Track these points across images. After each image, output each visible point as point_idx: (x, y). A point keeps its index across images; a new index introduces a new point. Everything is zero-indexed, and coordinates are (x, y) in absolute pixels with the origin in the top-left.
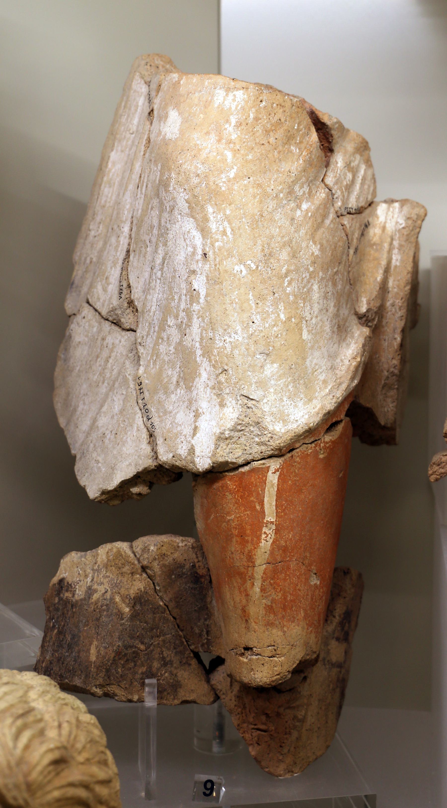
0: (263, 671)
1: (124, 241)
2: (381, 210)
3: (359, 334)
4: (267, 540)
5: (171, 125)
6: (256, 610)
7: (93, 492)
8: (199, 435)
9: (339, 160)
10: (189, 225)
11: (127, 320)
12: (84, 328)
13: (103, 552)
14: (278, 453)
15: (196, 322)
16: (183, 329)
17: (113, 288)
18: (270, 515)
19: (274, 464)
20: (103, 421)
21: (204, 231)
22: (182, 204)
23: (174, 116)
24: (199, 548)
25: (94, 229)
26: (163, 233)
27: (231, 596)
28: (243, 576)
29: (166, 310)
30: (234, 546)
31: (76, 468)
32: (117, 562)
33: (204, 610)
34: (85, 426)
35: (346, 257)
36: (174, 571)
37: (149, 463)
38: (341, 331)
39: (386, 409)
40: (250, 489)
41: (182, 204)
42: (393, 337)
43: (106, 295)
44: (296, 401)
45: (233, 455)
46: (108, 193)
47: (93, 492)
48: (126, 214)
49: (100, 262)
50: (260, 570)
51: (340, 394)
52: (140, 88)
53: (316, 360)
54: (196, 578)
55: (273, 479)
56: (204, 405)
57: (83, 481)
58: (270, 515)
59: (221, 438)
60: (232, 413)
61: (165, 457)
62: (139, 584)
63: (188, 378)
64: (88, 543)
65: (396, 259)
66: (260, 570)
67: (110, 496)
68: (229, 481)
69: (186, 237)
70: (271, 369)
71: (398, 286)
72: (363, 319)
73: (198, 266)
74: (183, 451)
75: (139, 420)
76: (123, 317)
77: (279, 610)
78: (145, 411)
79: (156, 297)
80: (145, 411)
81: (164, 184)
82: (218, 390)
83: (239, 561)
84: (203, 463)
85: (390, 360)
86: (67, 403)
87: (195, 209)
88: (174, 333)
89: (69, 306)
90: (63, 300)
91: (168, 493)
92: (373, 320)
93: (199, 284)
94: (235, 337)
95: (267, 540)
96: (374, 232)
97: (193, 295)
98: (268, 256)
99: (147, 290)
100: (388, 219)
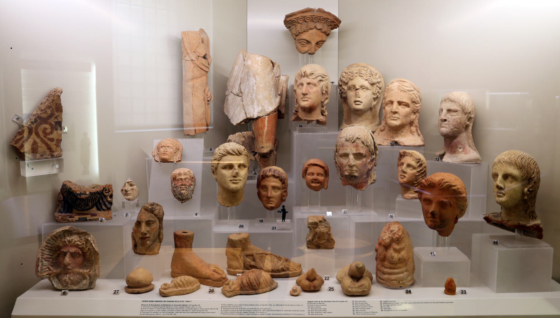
0: (265, 151)
1: (239, 82)
2: (281, 77)
3: (279, 97)
4: (266, 129)
5: (249, 63)
6: (264, 141)
7: (235, 124)
8: (254, 113)
9: (275, 68)
10: (253, 78)
11: (240, 95)
12: (231, 97)
13: (237, 134)
14: (268, 115)
15: (254, 95)
16: (251, 96)
17: (237, 89)
18: (266, 125)
19: (267, 117)
20: (236, 112)
21: (256, 80)
22: (252, 75)
23: (249, 61)
24: (253, 133)
25: (232, 80)
26: (248, 80)
27: (260, 139)
28: (261, 135)
29: (248, 93)
30: (260, 130)
31: (18, 298)
32: (239, 136)
33: (254, 144)
34: (232, 114)
35: (276, 85)
36: (249, 137)
37: (245, 118)
38: (276, 96)
39: (283, 111)
40: (263, 121)
41: (252, 75)
42: (284, 99)
43: (236, 91)
44: (270, 105)
45: (261, 115)
46: (235, 73)
47: (235, 124)
48: (240, 77)
49: (234, 85)
50: (265, 134)
51: (277, 106)
52: (241, 56)
53: (273, 100)
54: (252, 138)
55: (267, 119)
56: (255, 107)
57: (232, 123)
58: (266, 125)
59: (259, 112)
60: (260, 108)
61: (248, 116)
62: (243, 139)
63: (252, 103)
64: (234, 133)
65: (284, 85)
66: (265, 134)
67: (238, 124)
68: (260, 120)
69: (252, 81)
70: (266, 101)
71: (284, 90)
72: (279, 95)
73: (255, 85)
74: (252, 115)
75: (243, 111)
76: (240, 94)
77: (268, 140)
78: (244, 109)
79: (247, 90)
80: (244, 109)
81: (248, 72)
82: (258, 105)
83: (261, 133)
84: (255, 117)
85: (283, 103)
86: (227, 110)
87: (254, 76)
88: (250, 96)
89: (226, 93)
90: (225, 92)
91: (249, 122)
92: (281, 95)
93: (255, 88)
94: (260, 96)
95: (266, 129)
96: (280, 81)
97: (254, 90)
98: (266, 84)
99: (245, 89)
100: (283, 78)
